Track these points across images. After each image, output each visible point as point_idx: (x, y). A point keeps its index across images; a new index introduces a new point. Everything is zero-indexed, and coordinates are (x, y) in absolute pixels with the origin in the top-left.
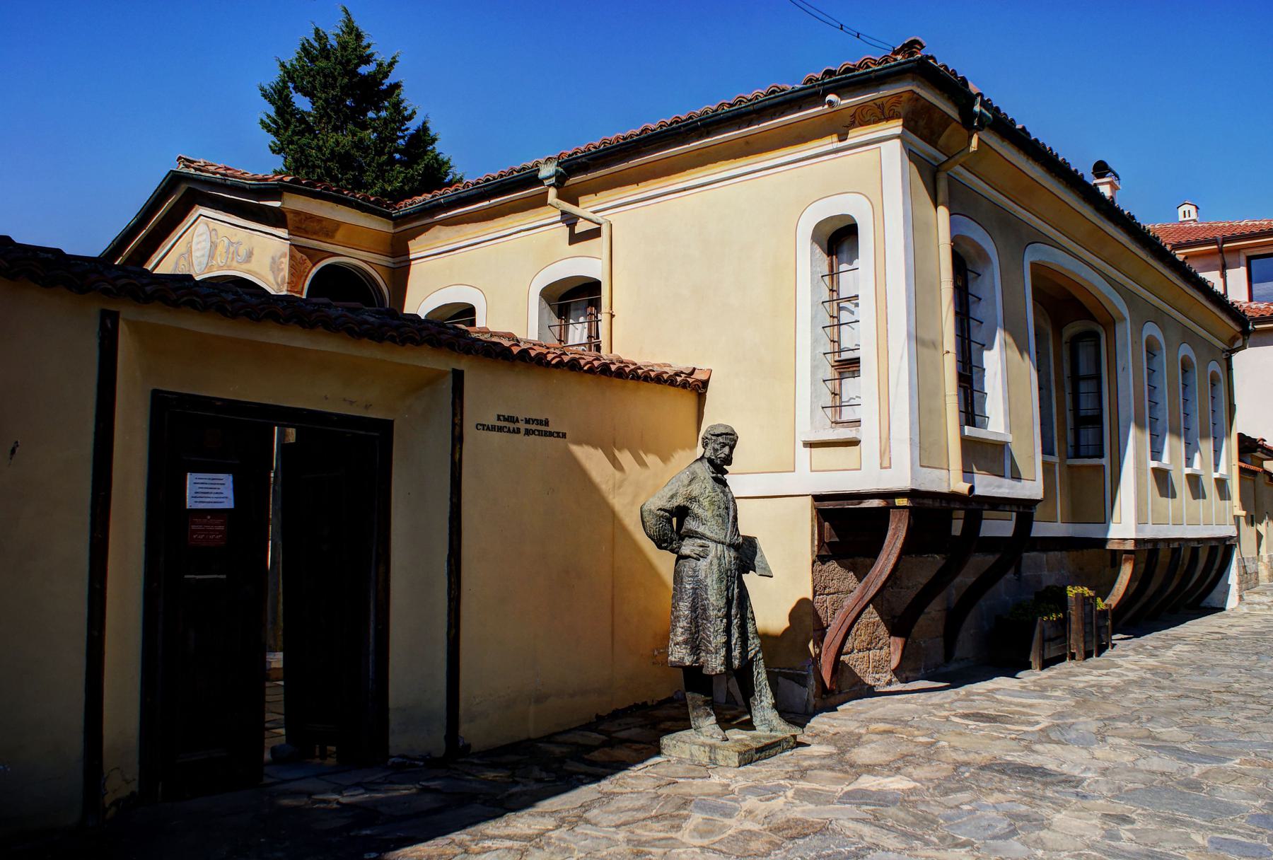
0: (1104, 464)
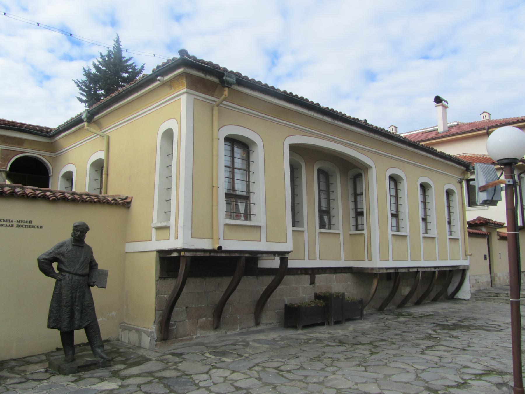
0: (364, 233)
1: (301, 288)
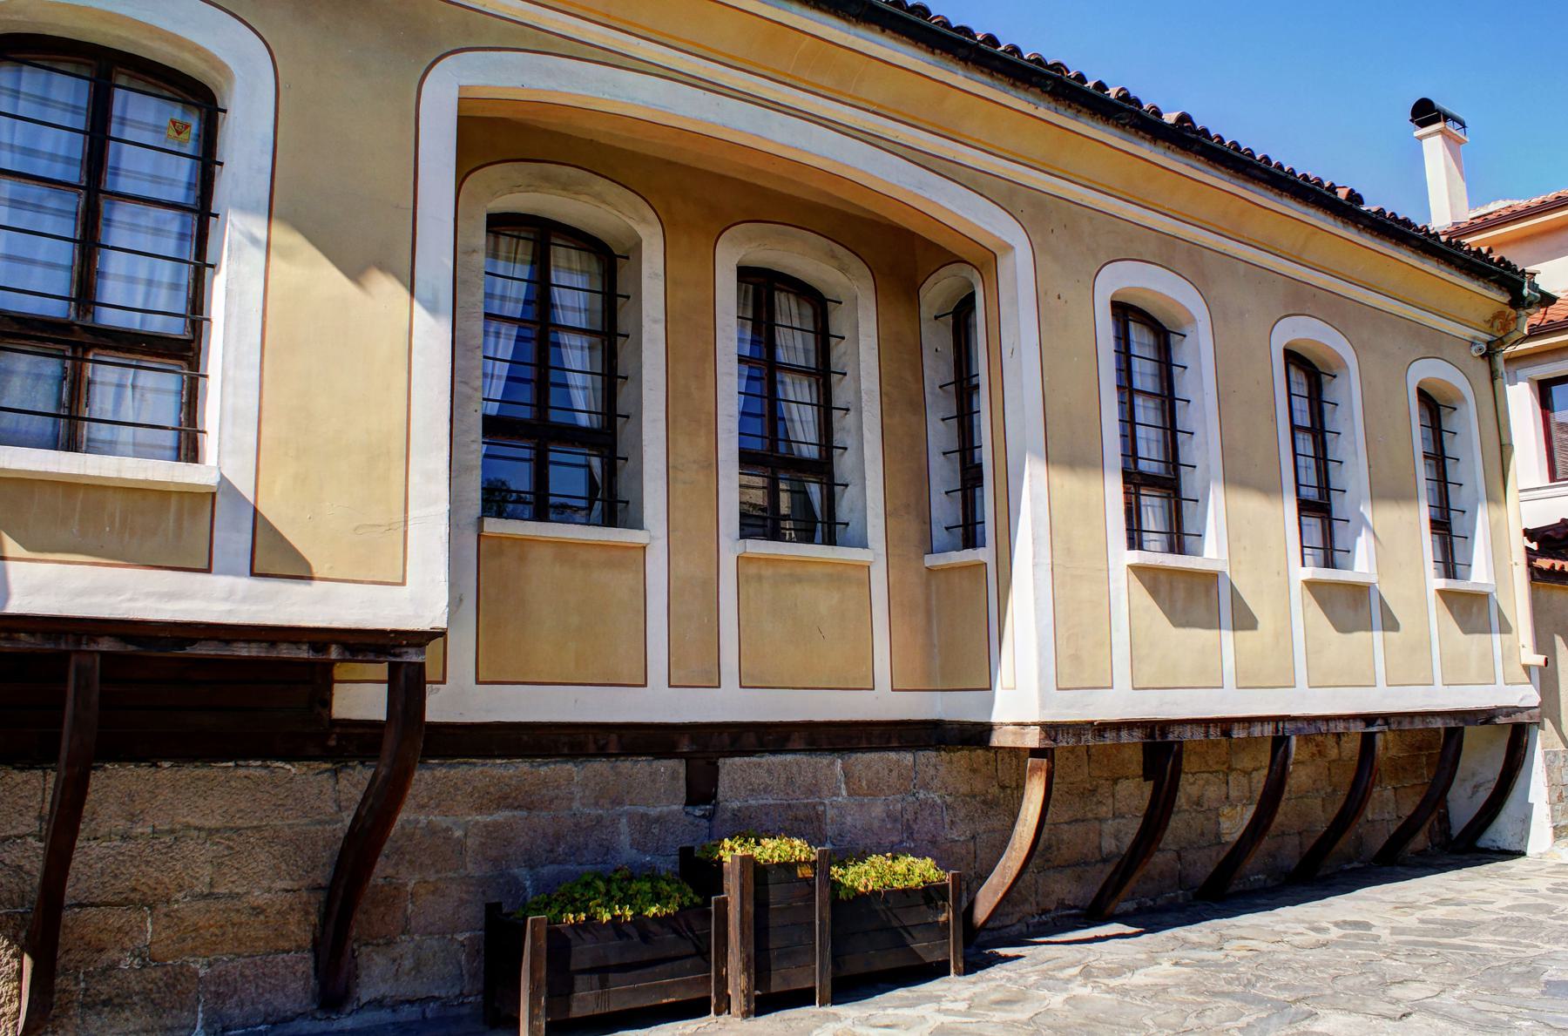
1: (624, 820)
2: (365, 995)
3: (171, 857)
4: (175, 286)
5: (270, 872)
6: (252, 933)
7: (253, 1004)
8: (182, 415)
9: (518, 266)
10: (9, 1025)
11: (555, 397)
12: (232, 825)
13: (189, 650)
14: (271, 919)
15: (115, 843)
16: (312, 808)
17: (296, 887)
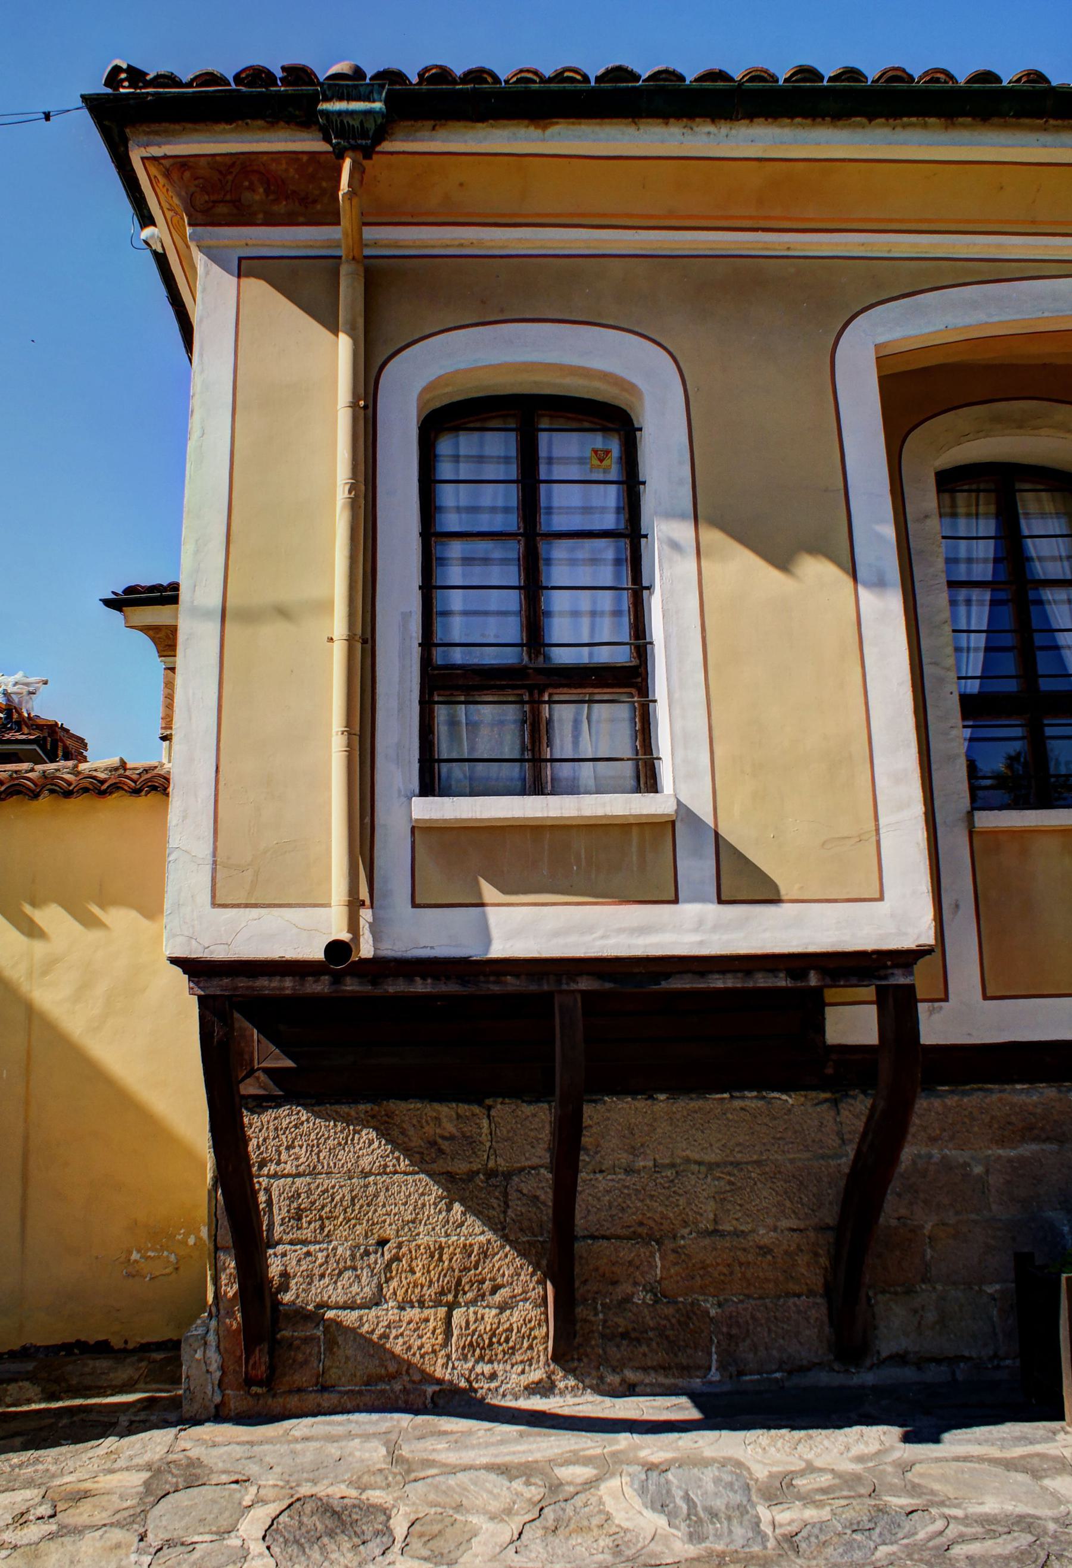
2: (886, 1347)
3: (674, 1192)
4: (617, 613)
5: (774, 1210)
6: (761, 1274)
7: (766, 1349)
8: (638, 743)
9: (981, 522)
10: (541, 1348)
11: (1044, 663)
12: (731, 1159)
13: (665, 985)
14: (779, 1260)
15: (619, 1176)
16: (814, 1141)
17: (802, 1226)
